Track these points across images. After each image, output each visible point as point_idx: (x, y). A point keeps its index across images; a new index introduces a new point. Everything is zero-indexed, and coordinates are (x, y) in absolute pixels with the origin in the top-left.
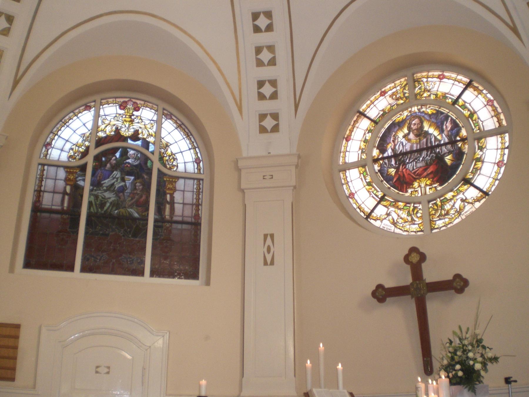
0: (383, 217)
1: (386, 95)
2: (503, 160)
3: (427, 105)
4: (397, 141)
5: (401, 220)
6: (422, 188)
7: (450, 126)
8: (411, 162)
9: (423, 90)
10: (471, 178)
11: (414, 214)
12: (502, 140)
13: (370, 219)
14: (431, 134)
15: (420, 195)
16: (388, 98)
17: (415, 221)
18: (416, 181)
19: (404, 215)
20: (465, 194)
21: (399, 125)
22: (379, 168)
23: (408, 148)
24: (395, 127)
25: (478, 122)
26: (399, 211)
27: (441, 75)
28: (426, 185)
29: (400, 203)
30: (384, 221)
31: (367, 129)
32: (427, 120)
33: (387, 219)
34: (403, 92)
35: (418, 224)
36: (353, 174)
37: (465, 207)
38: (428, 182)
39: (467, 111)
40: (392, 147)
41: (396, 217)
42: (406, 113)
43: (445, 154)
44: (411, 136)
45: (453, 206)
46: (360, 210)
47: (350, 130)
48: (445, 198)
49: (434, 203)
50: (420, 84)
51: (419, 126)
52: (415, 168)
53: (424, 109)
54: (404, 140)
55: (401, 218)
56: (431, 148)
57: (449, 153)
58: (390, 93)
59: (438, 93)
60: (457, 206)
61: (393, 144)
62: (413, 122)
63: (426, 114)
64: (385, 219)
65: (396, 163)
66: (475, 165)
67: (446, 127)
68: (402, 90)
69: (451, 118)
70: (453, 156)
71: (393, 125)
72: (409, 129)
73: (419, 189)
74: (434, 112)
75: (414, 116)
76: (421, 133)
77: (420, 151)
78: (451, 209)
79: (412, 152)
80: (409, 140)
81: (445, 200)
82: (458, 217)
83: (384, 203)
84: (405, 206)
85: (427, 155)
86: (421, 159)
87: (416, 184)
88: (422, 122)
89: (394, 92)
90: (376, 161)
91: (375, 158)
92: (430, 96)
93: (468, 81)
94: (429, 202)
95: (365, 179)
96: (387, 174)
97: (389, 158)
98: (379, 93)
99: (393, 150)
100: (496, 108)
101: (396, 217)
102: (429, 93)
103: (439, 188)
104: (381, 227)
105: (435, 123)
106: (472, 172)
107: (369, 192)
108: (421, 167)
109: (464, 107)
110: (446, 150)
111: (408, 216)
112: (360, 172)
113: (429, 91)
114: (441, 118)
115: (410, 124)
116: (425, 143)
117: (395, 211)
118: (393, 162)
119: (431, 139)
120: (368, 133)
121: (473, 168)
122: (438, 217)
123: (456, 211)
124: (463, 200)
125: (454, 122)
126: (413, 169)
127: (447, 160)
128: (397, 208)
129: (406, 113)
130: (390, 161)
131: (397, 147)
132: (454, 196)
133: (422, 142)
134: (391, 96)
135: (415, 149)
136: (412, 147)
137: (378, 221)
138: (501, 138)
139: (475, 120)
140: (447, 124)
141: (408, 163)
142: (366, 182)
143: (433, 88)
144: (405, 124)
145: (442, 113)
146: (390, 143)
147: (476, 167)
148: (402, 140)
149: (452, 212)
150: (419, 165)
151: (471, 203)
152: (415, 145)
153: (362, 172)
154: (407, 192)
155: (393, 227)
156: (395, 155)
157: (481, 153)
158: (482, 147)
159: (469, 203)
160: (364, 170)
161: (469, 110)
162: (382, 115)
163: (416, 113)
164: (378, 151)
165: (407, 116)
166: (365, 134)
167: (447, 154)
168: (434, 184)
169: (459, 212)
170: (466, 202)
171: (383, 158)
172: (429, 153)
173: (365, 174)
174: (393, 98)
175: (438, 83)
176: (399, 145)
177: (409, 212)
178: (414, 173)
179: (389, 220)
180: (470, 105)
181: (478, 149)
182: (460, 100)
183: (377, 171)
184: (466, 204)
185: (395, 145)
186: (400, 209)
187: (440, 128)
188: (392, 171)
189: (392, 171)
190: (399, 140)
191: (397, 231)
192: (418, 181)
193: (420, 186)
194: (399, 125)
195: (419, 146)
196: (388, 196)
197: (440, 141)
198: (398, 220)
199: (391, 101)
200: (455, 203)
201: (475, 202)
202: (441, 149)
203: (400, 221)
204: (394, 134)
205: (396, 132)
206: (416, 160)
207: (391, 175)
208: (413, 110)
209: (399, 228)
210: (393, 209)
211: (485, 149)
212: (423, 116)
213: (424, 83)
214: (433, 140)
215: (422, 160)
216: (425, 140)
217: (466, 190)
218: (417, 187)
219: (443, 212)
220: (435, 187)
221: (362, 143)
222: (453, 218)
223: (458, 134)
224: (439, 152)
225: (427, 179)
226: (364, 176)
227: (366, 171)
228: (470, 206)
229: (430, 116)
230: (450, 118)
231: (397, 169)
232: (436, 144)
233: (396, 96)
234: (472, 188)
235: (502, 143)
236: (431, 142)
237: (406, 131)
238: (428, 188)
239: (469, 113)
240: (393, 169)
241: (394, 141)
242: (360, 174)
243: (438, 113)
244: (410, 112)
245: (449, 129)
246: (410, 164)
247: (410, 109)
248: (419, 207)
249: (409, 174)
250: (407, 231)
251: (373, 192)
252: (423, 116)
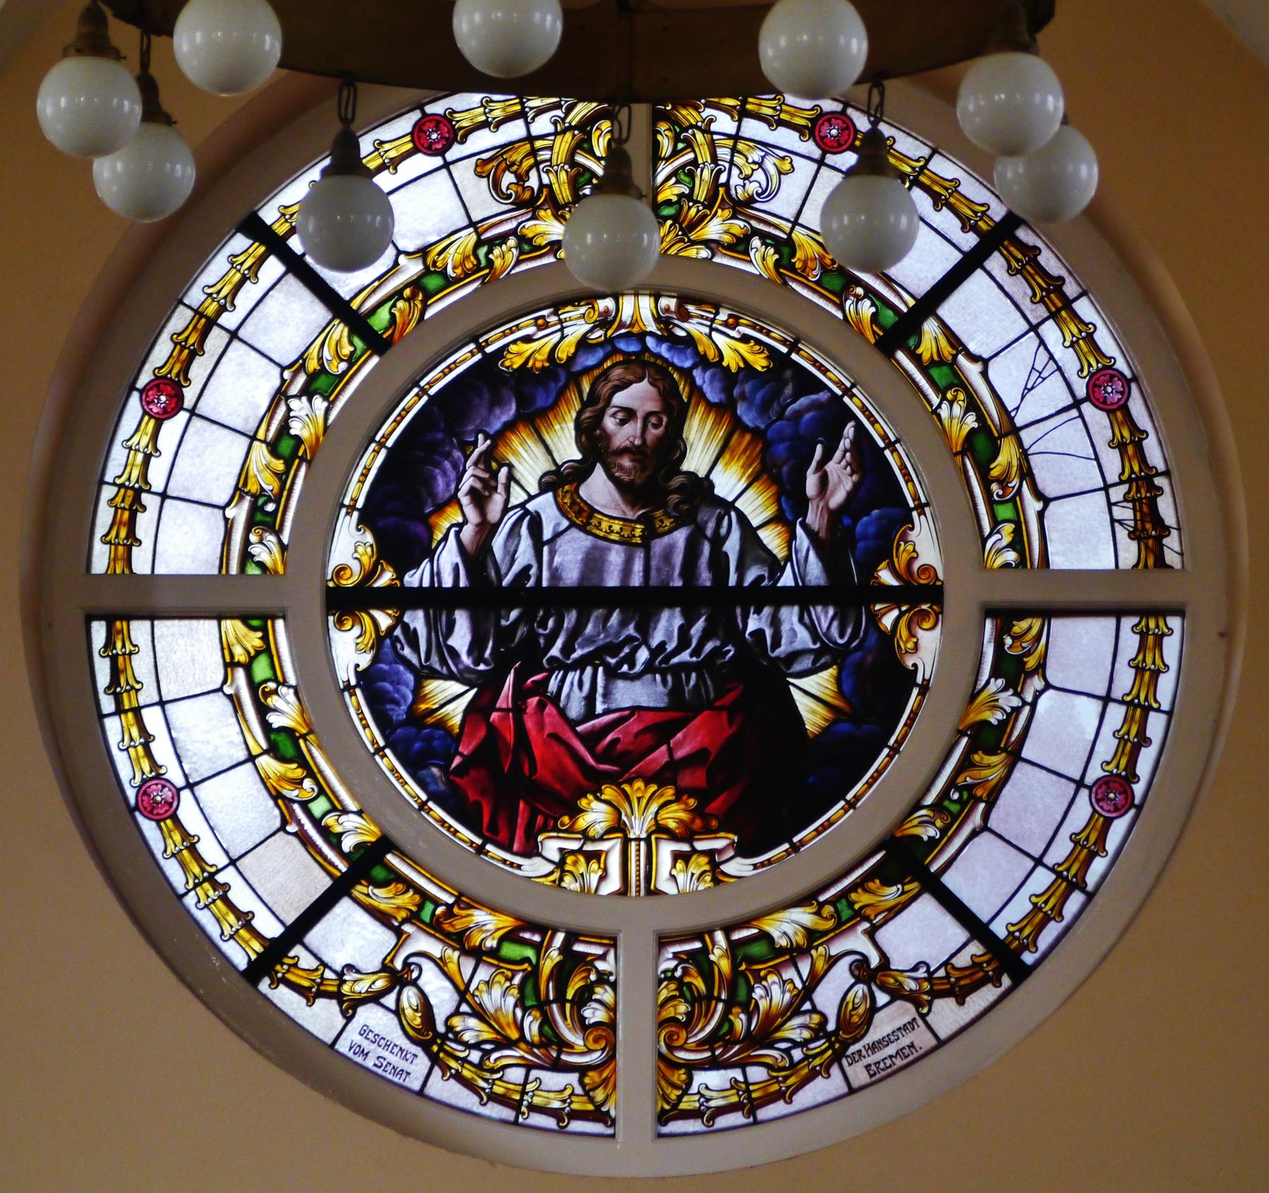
0: (362, 987)
1: (455, 152)
2: (1132, 776)
3: (717, 307)
4: (498, 499)
5: (473, 1022)
6: (629, 860)
7: (848, 484)
8: (580, 665)
9: (701, 193)
10: (933, 842)
11: (561, 999)
12: (1142, 647)
13: (275, 983)
14: (728, 506)
15: (613, 884)
16: (465, 172)
17: (564, 1045)
18: (597, 793)
19: (499, 998)
20: (883, 935)
21: (532, 394)
22: (365, 661)
23: (570, 556)
24: (497, 402)
25: (1016, 500)
26: (468, 965)
27: (829, 117)
28: (660, 829)
29: (480, 916)
30: (368, 1015)
31: (299, 364)
32: (710, 406)
33: (390, 1000)
34: (571, 161)
35: (582, 1070)
36: (183, 655)
37: (874, 1009)
38: (674, 816)
39: (957, 410)
40: (468, 533)
41: (442, 997)
42: (577, 324)
43: (795, 656)
44: (598, 489)
45: (808, 991)
46: (109, 644)
47: (178, 342)
48: (765, 936)
49: (690, 954)
50: (690, 145)
51: (653, 432)
52: (600, 708)
53: (695, 328)
54: (545, 505)
55: (479, 1013)
56: (717, 603)
57: (825, 654)
58: (482, 141)
59: (799, 235)
60: (828, 997)
61: (472, 515)
62: (620, 399)
63: (702, 361)
64: (375, 998)
65: (476, 648)
66: (966, 764)
67: (824, 481)
68: (563, 144)
69: (859, 427)
70: (838, 680)
71: (488, 377)
72: (590, 434)
73: (612, 847)
74: (760, 362)
75: (627, 354)
76: (659, 485)
77: (641, 603)
78: (793, 1009)
79: (589, 596)
80: (581, 516)
81: (758, 949)
82: (825, 1070)
83: (383, 898)
84: (511, 936)
85: (684, 642)
86: (643, 655)
87: (595, 814)
88: (673, 412)
89: (510, 146)
90: (346, 602)
91: (348, 582)
92: (740, 246)
93: (998, 212)
94: (663, 941)
95: (263, 710)
96: (411, 709)
97: (437, 601)
98: (405, 124)
99: (476, 557)
100: (1138, 435)
101: (442, 997)
102: (738, 226)
103: (737, 867)
104: (342, 1047)
105: (757, 434)
106: (937, 807)
107: (277, 796)
108: (635, 709)
109: (948, 371)
110: (804, 638)
111: (520, 1002)
112: (226, 648)
113: (740, 207)
114: (798, 414)
115: (596, 405)
116: (678, 559)
117: (440, 964)
118: (461, 638)
119: (718, 541)
120: (308, 392)
121: (951, 784)
122: (709, 1042)
123: (819, 1031)
124: (862, 970)
125: (868, 458)
126: (590, 713)
127: (804, 705)
128: (459, 941)
129: (577, 324)
130: (441, 629)
131: (498, 543)
132: (812, 935)
133: (658, 545)
134: (491, 166)
135: (612, 581)
136: (593, 562)
137: (321, 1002)
138: (1143, 635)
139: (1003, 481)
140: (831, 467)
141: (556, 664)
142: (267, 728)
143: (768, 193)
144: (559, 398)
145: (808, 383)
146: (454, 500)
147: (967, 779)
148: (532, 495)
149: (794, 1030)
150: (630, 694)
151: (913, 998)
152: (616, 557)
153: (240, 655)
154: (532, 851)
155: (423, 1062)
156: (482, 590)
157: (1009, 700)
158: (1020, 660)
159: (897, 994)
160: (254, 640)
161: (973, 405)
162: (416, 284)
163: (643, 335)
164: (369, 538)
165: (583, 344)
166: (280, 395)
167: (806, 663)
168: (709, 832)
169: (844, 1035)
170: (884, 988)
171: (399, 599)
172: (697, 629)
173: (261, 669)
174: (496, 185)
175: (805, 169)
176: (514, 532)
177: (533, 974)
178: (591, 739)
179: (398, 1012)
180: (984, 374)
181: (995, 674)
182: (930, 327)
183: (345, 673)
184: (882, 998)
185: (487, 530)
186: (478, 954)
187: (781, 473)
188: (450, 699)
189: (450, 699)
190: (517, 496)
191: (442, 1088)
192: (609, 792)
193: (618, 827)
194: (532, 394)
195: (638, 566)
196: (403, 855)
197: (776, 567)
198: (457, 1022)
199: (484, 203)
200: (815, 980)
201: (936, 994)
202: (775, 622)
203: (472, 1029)
204: (483, 445)
205: (498, 438)
206: (610, 660)
207: (442, 724)
208: (627, 313)
209: (458, 1077)
210: (435, 948)
211: (1037, 683)
212: (687, 374)
213: (713, 146)
214: (732, 547)
215: (649, 667)
216: (680, 536)
217: (895, 911)
218: (599, 829)
219: (739, 1021)
220: (710, 854)
221: (260, 453)
222: (793, 1065)
223: (883, 550)
224: (759, 633)
225: (669, 793)
226: (253, 686)
227: (267, 649)
228: (902, 1012)
229: (728, 378)
230: (849, 430)
231: (486, 687)
232: (750, 577)
233: (522, 178)
234: (926, 906)
235: (1139, 670)
236: (719, 561)
237: (566, 445)
238: (666, 850)
239: (971, 421)
240: (455, 687)
241: (480, 499)
242: (230, 664)
243: (783, 373)
244: (605, 321)
245: (837, 498)
246: (573, 676)
247: (606, 304)
248: (600, 965)
249: (554, 737)
250: (502, 1100)
251: (305, 805)
252: (687, 374)
